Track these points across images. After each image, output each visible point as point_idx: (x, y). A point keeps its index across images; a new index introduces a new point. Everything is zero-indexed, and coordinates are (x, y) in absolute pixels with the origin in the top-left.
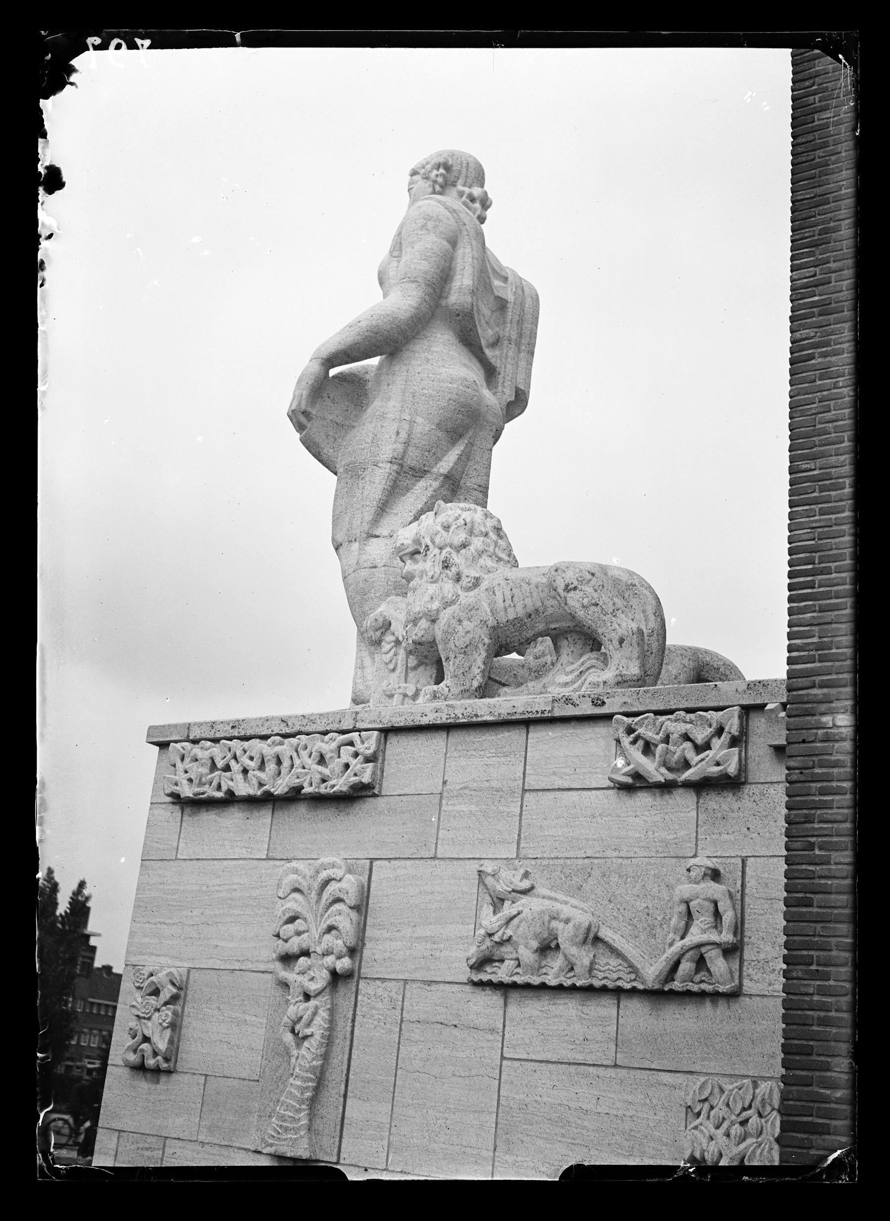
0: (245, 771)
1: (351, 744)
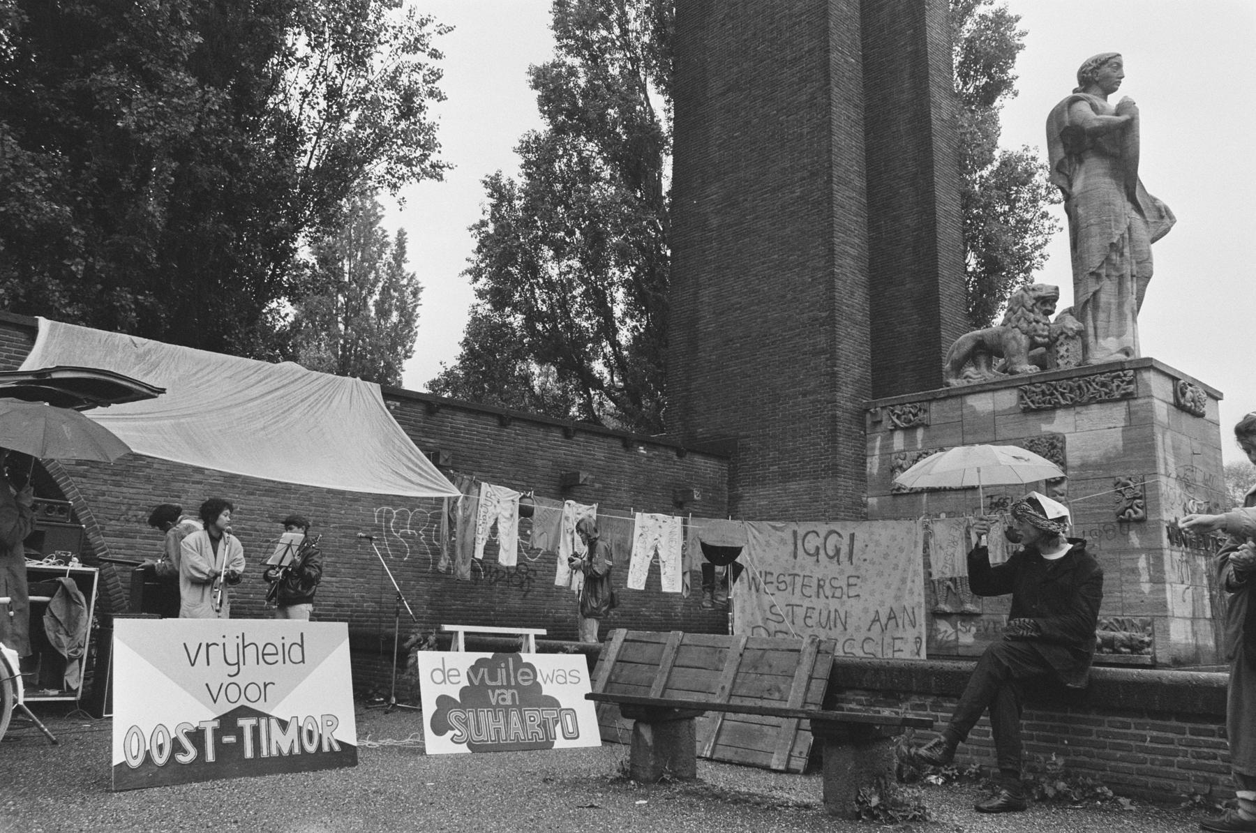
0: (1062, 394)
1: (1119, 376)
